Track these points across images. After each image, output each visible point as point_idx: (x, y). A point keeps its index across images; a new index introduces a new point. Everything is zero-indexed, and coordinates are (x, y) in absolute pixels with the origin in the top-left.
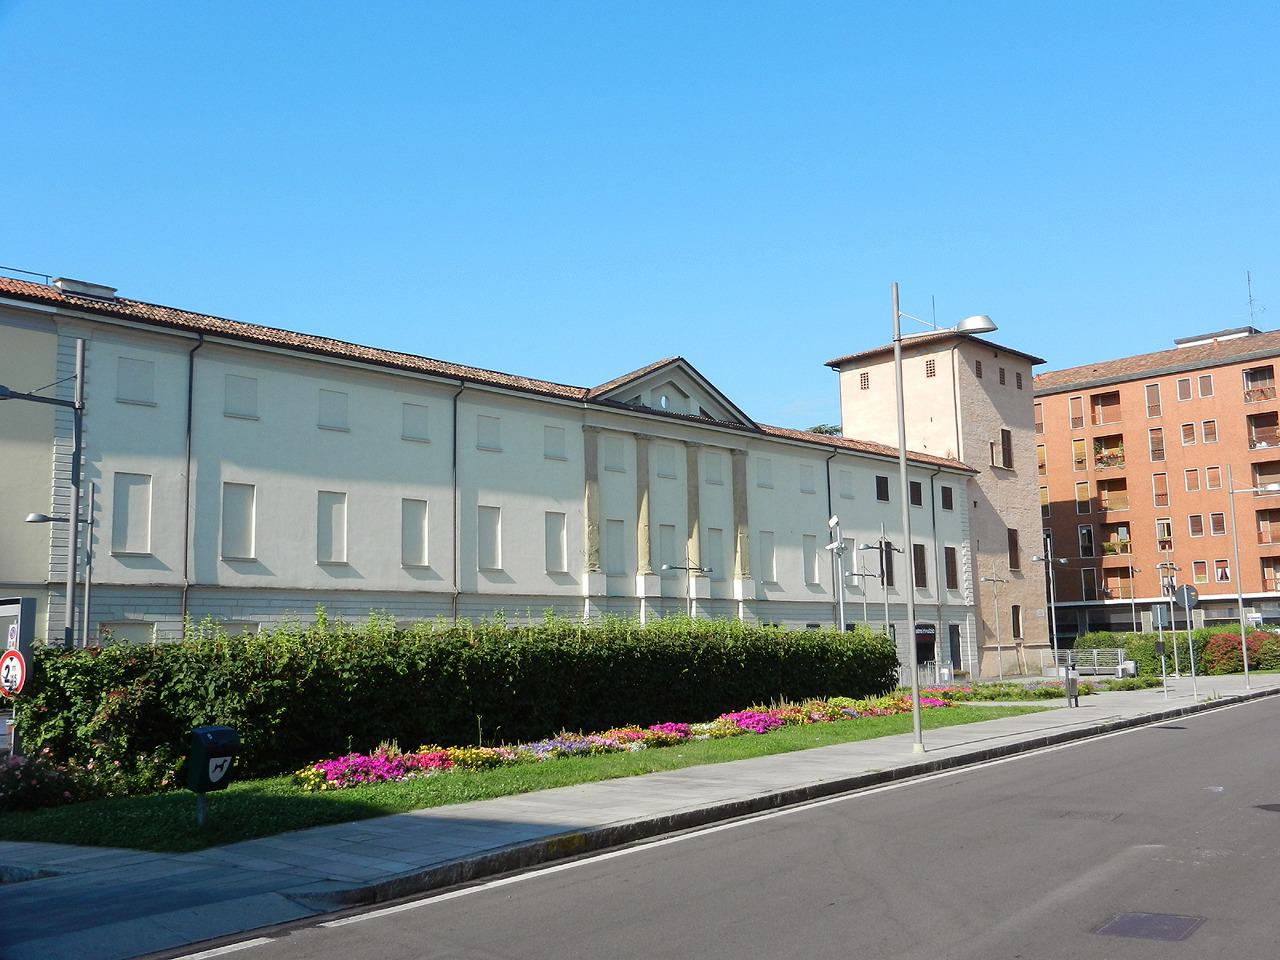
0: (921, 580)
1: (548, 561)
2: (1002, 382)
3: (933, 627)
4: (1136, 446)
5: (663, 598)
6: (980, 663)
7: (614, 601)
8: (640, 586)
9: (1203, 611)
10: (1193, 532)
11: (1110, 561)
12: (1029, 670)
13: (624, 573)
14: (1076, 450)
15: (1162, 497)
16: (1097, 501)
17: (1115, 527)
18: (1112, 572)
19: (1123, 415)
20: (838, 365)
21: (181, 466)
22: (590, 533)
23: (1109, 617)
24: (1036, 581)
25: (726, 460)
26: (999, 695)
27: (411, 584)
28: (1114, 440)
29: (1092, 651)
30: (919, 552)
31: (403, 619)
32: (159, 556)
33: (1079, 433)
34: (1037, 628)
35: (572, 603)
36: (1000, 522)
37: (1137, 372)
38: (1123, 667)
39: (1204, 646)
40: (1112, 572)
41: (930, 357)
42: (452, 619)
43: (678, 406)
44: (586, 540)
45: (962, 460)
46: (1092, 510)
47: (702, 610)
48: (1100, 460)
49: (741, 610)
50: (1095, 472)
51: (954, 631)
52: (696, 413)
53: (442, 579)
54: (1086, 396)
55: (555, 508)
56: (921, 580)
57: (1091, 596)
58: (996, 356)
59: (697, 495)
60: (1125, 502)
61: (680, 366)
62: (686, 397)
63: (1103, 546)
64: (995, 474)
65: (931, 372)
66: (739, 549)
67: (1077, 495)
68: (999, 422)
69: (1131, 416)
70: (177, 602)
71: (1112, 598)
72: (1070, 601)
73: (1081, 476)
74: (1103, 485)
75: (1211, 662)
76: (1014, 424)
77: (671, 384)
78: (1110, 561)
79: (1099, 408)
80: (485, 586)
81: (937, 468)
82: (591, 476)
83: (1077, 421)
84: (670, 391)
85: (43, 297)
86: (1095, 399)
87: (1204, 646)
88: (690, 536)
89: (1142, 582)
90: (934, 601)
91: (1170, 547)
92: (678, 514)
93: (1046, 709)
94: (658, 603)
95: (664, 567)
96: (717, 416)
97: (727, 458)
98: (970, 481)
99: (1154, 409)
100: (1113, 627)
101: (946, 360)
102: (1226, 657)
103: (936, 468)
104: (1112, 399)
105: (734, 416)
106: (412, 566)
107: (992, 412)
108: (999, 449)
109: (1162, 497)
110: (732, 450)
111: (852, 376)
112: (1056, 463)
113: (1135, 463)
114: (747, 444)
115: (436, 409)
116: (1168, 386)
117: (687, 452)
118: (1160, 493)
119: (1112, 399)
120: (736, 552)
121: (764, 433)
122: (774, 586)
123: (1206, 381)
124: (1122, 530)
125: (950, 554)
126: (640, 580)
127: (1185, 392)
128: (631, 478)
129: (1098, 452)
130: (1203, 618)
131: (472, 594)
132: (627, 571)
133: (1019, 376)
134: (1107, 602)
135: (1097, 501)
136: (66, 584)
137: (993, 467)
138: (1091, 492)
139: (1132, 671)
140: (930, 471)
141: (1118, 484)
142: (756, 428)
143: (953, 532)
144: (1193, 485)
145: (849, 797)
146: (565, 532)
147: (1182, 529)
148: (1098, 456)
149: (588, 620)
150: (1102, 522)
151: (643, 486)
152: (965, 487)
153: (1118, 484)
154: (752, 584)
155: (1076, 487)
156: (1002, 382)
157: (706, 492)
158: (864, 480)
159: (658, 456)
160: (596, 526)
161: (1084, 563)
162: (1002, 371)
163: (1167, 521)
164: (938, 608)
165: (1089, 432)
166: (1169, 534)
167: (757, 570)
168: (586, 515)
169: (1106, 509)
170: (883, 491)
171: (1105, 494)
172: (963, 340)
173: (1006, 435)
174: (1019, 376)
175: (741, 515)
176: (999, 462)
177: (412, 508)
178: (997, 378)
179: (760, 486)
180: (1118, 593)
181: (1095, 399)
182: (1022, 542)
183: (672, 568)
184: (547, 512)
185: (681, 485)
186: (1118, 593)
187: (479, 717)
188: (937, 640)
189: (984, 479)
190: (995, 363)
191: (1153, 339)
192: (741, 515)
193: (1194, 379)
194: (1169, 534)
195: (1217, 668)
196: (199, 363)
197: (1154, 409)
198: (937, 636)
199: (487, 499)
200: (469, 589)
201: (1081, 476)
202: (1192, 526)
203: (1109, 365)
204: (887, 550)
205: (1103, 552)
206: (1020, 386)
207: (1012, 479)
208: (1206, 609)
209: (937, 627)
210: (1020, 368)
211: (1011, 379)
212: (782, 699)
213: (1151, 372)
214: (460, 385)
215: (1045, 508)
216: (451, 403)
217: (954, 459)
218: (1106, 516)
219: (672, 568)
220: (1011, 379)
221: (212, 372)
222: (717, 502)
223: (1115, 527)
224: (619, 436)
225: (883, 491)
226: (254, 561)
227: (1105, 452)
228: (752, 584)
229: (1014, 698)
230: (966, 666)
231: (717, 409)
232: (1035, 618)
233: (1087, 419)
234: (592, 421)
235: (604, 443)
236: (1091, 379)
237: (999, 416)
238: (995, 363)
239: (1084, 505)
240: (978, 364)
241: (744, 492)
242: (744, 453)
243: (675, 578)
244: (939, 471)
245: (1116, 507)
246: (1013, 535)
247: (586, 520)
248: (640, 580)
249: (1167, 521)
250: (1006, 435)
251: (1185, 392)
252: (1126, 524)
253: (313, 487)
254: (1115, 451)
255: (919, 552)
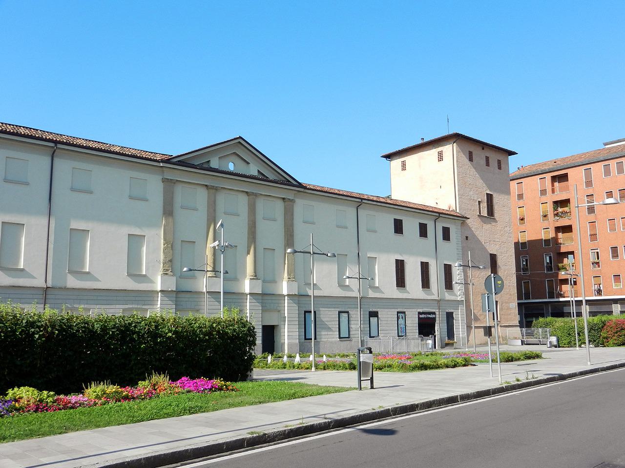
0: (426, 283)
1: (120, 264)
2: (488, 164)
3: (434, 313)
4: (579, 204)
5: (263, 294)
6: (468, 336)
7: (180, 296)
8: (246, 286)
9: (619, 306)
10: (612, 257)
11: (562, 275)
12: (503, 340)
13: (194, 276)
14: (542, 209)
15: (593, 236)
16: (555, 239)
17: (566, 254)
18: (565, 282)
19: (571, 188)
20: (389, 157)
21: (45, 221)
22: (165, 249)
23: (563, 308)
24: (509, 286)
25: (279, 206)
26: (385, 367)
27: (131, 285)
28: (565, 203)
29: (547, 330)
30: (425, 267)
31: (127, 306)
32: (27, 269)
33: (544, 199)
34: (510, 314)
35: (148, 296)
36: (485, 250)
37: (579, 161)
38: (550, 340)
39: (603, 327)
40: (565, 282)
41: (440, 149)
42: (42, 306)
43: (242, 169)
44: (162, 254)
45: (458, 211)
46: (552, 245)
47: (254, 301)
48: (557, 215)
49: (286, 301)
50: (554, 222)
51: (450, 316)
52: (256, 174)
53: (100, 281)
54: (548, 177)
55: (137, 231)
56: (426, 283)
57: (551, 296)
58: (483, 149)
59: (255, 227)
60: (572, 239)
61: (240, 142)
62: (248, 163)
63: (558, 266)
64: (482, 220)
65: (440, 157)
66: (286, 262)
67: (543, 236)
68: (485, 189)
69: (575, 188)
70: (41, 296)
71: (564, 297)
72: (541, 299)
73: (545, 224)
74: (558, 229)
75: (607, 338)
76: (495, 191)
77: (235, 153)
78: (562, 275)
79: (556, 184)
80: (72, 282)
81: (438, 215)
82: (168, 211)
83: (543, 192)
84: (234, 158)
85: (28, 135)
86: (554, 179)
87: (603, 327)
88: (248, 253)
89: (581, 284)
90: (435, 297)
91: (599, 266)
92: (240, 237)
93: (327, 390)
94: (296, 298)
95: (185, 269)
96: (271, 177)
97: (280, 205)
98: (463, 223)
99: (589, 183)
100: (565, 315)
101: (449, 150)
102: (616, 335)
103: (437, 215)
104: (563, 178)
105: (284, 177)
106: (134, 273)
107: (480, 182)
108: (484, 205)
109: (593, 236)
110: (284, 199)
111: (396, 163)
112: (526, 215)
113: (577, 217)
114: (294, 194)
115: (36, 164)
116: (597, 169)
117: (208, 193)
118: (592, 233)
119: (563, 178)
120: (285, 264)
121: (305, 188)
122: (377, 289)
123: (620, 165)
124: (570, 256)
125: (448, 269)
126: (247, 282)
127: (607, 172)
128: (202, 214)
129: (555, 210)
130: (619, 309)
131: (60, 288)
132: (196, 275)
133: (499, 162)
134: (561, 299)
135: (555, 239)
136: (220, 292)
137: (480, 216)
138: (551, 234)
139: (555, 343)
140: (435, 217)
141: (568, 229)
142: (300, 185)
143: (450, 253)
144: (613, 229)
145: (528, 390)
146: (144, 249)
147: (606, 256)
148: (556, 212)
149: (159, 310)
150: (559, 252)
151: (212, 219)
152: (459, 227)
153: (568, 229)
154: (295, 285)
155: (539, 230)
156: (488, 164)
157: (262, 226)
158: (387, 220)
159: (223, 201)
160: (170, 245)
161: (547, 276)
162: (487, 159)
163: (597, 251)
164: (438, 301)
165: (550, 198)
166: (598, 258)
167: (298, 275)
168: (162, 238)
169: (561, 244)
170: (398, 227)
171: (560, 235)
172: (457, 137)
173: (490, 197)
174: (499, 162)
175: (289, 240)
176: (485, 213)
177: (135, 241)
178: (484, 162)
179: (182, 207)
180: (568, 294)
181: (554, 179)
182: (500, 262)
183: (191, 270)
184: (129, 234)
185: (242, 221)
186: (568, 294)
187: (6, 373)
188: (437, 321)
189: (474, 223)
190: (484, 155)
191: (591, 145)
192: (289, 240)
193: (613, 164)
194: (598, 258)
195: (611, 342)
196: (56, 160)
197: (589, 183)
198: (437, 319)
199: (75, 225)
200: (59, 284)
201: (545, 224)
202: (612, 253)
203: (563, 159)
204: (400, 266)
205: (559, 269)
206: (500, 168)
207: (494, 224)
208: (621, 304)
209: (437, 313)
210: (501, 157)
211: (493, 163)
212: (153, 373)
213: (587, 162)
214: (56, 146)
215: (517, 244)
216: (49, 159)
217: (453, 211)
218: (560, 248)
219: (191, 270)
220: (493, 163)
221: (65, 166)
222: (271, 232)
223: (566, 254)
224: (193, 186)
225: (398, 227)
226: (88, 273)
227: (560, 210)
228: (295, 285)
229: (494, 360)
230: (458, 338)
231: (273, 173)
232: (509, 308)
233: (549, 190)
234: (169, 175)
235: (179, 190)
236: (551, 167)
237: (484, 185)
238: (484, 155)
239: (547, 241)
240: (471, 154)
241: (292, 225)
242: (292, 201)
243: (194, 277)
244: (439, 217)
245: (566, 243)
246: (493, 258)
247: (162, 241)
248: (247, 282)
249: (597, 251)
250: (490, 197)
251: (607, 172)
252: (572, 253)
253: (126, 230)
254: (566, 209)
255: (425, 267)
